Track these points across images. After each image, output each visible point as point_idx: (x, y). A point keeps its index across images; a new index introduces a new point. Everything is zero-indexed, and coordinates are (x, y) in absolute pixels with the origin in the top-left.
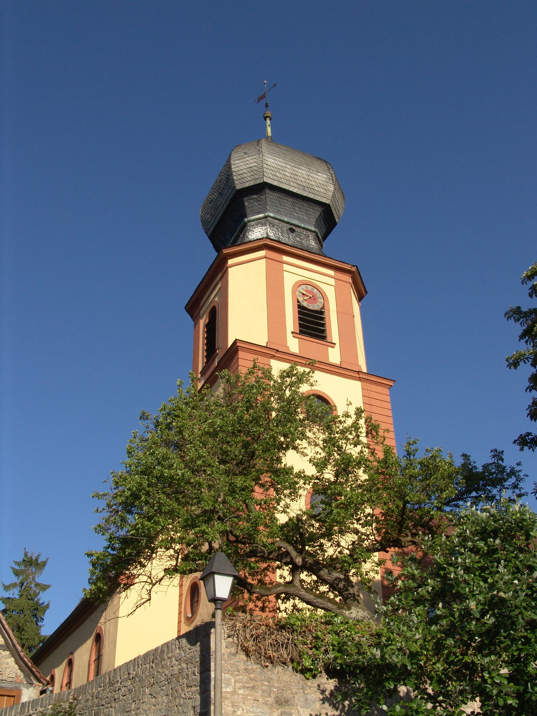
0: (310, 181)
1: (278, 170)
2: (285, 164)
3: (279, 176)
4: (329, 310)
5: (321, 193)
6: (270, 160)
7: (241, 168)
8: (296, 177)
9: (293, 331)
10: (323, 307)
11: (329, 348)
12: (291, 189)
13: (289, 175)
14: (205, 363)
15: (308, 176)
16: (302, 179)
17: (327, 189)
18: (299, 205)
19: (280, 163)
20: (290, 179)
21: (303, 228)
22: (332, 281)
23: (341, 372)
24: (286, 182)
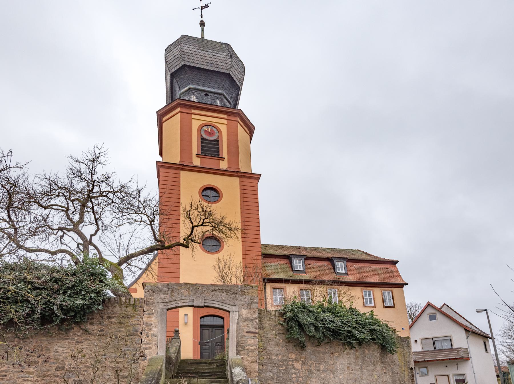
1: (192, 54)
2: (196, 50)
7: (170, 58)
8: (204, 58)
9: (197, 153)
11: (221, 161)
12: (202, 67)
14: (250, 134)
16: (209, 59)
17: (227, 63)
18: (210, 78)
20: (201, 60)
21: (215, 93)
22: (225, 122)
23: (226, 173)
24: (198, 62)
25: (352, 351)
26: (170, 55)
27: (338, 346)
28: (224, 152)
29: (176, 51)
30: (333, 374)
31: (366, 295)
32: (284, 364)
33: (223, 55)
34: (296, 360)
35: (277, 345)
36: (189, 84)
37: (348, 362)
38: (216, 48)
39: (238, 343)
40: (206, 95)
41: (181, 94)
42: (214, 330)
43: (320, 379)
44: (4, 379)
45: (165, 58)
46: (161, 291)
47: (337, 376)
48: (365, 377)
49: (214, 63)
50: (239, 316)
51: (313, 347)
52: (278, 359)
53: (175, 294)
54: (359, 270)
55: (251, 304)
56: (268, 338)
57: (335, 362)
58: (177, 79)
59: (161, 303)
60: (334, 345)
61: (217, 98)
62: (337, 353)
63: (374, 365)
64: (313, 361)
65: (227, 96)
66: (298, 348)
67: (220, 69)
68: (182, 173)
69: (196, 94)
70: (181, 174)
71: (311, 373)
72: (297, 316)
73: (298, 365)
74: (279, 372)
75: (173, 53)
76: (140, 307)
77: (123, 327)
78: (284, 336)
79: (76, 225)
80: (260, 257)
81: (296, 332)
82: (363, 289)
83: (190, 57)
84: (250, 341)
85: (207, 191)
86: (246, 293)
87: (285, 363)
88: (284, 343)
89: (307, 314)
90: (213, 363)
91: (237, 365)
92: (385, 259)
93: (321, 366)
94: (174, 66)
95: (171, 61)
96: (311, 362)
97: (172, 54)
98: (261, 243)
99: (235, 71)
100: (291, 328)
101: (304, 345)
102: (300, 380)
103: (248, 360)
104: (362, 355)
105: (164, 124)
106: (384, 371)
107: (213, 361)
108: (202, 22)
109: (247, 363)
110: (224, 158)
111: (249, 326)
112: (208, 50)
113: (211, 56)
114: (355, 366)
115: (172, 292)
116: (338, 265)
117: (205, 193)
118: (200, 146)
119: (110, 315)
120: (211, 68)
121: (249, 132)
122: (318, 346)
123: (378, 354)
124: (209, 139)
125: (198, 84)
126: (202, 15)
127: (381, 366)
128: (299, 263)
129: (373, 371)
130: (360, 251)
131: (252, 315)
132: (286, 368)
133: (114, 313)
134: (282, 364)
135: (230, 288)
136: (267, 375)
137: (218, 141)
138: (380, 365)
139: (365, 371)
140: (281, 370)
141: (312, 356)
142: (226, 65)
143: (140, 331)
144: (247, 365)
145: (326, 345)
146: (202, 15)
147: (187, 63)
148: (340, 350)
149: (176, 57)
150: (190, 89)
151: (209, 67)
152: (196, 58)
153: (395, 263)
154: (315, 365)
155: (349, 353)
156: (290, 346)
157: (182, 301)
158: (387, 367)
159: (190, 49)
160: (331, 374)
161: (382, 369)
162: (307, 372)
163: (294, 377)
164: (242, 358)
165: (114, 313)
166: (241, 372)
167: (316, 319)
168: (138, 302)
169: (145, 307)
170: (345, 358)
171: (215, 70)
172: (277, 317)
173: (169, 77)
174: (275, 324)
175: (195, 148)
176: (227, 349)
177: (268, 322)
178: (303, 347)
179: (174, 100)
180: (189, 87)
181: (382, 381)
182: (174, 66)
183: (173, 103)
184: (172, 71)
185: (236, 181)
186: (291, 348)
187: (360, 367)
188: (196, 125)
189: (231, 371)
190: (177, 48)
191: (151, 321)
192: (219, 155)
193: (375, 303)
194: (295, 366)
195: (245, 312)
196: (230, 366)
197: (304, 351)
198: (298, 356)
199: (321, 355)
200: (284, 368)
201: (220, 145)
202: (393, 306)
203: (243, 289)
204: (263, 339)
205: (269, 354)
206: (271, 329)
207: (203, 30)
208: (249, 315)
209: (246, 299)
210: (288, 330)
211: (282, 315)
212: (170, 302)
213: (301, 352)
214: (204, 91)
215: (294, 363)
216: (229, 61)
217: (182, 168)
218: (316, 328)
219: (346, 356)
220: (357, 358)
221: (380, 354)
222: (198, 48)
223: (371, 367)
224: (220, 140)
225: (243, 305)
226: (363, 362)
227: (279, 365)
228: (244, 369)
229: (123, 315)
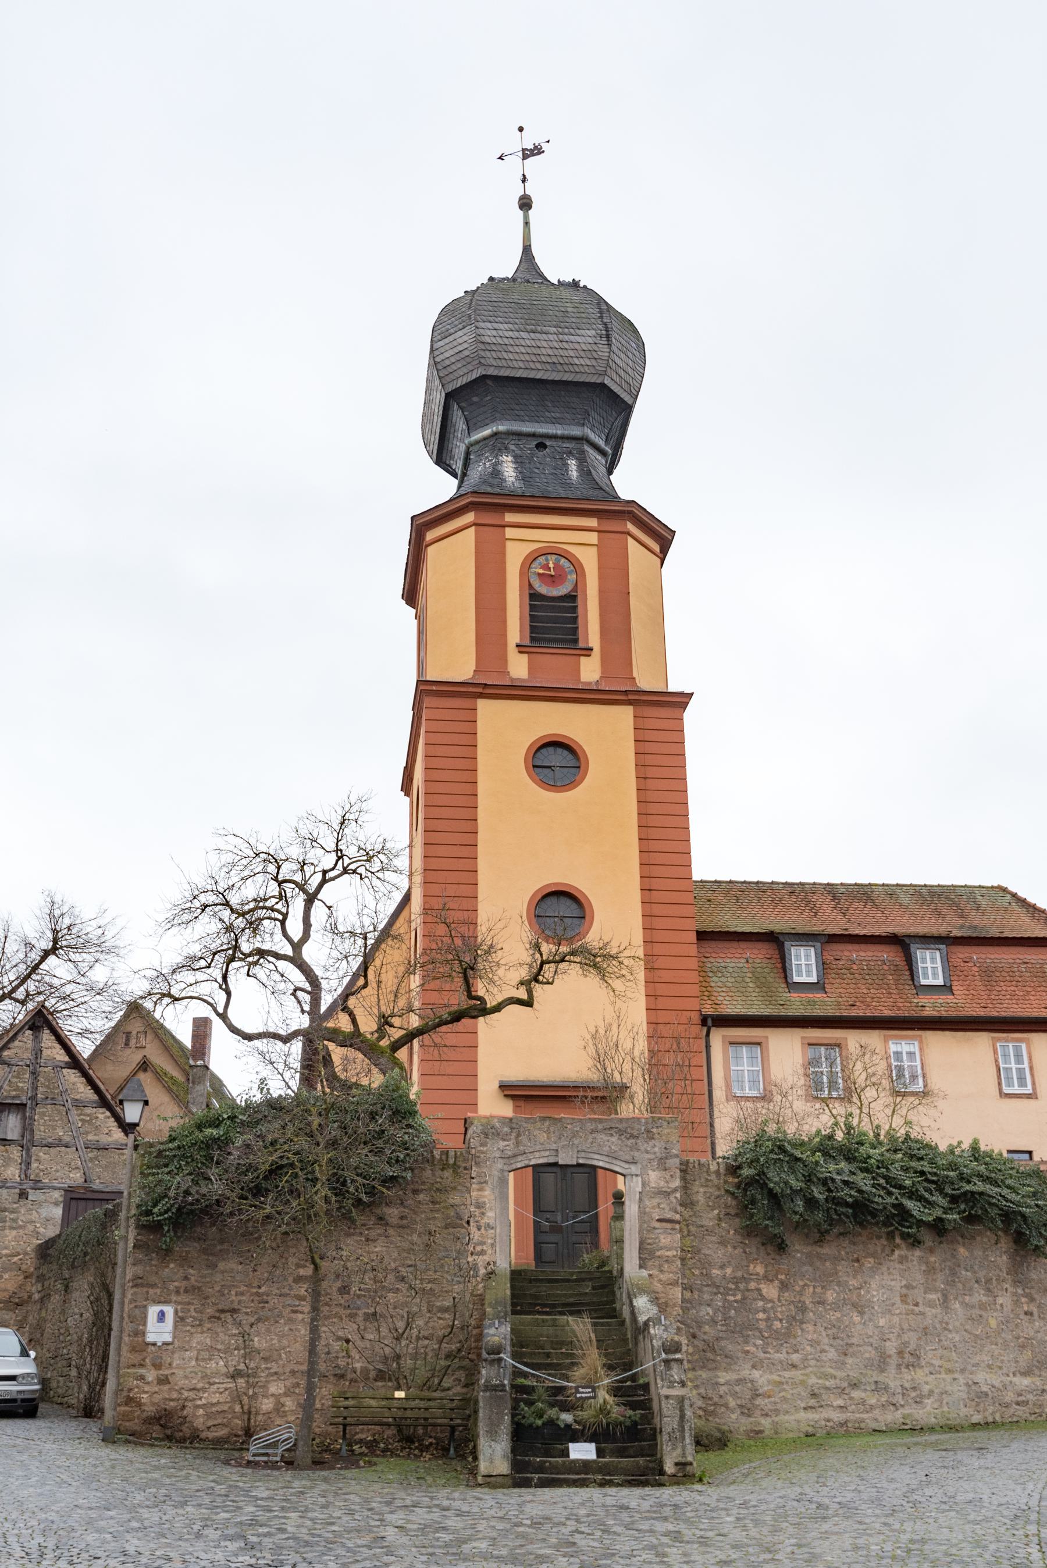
6: (489, 333)
7: (447, 355)
11: (582, 658)
12: (532, 375)
16: (550, 352)
19: (507, 334)
20: (527, 358)
21: (563, 438)
22: (593, 538)
24: (521, 364)
25: (918, 1253)
26: (447, 347)
27: (875, 1241)
28: (592, 632)
30: (861, 1313)
31: (1006, 1056)
32: (737, 1288)
33: (587, 336)
34: (767, 1278)
35: (723, 1243)
36: (494, 420)
37: (904, 1282)
38: (567, 319)
39: (641, 1243)
40: (541, 446)
41: (471, 445)
42: (569, 1175)
43: (825, 1325)
44: (263, 1307)
46: (498, 1134)
47: (870, 1320)
48: (957, 1324)
50: (644, 1184)
51: (808, 1244)
52: (724, 1277)
53: (523, 1139)
54: (988, 974)
55: (666, 1158)
56: (702, 1226)
57: (865, 1283)
58: (463, 404)
59: (500, 1160)
60: (864, 1238)
61: (570, 452)
62: (871, 1260)
63: (989, 1290)
64: (808, 1279)
66: (770, 1248)
67: (579, 376)
68: (482, 704)
69: (512, 447)
70: (479, 711)
71: (803, 1309)
72: (764, 1174)
73: (770, 1291)
74: (727, 1306)
76: (465, 1168)
77: (438, 1211)
78: (737, 1220)
79: (297, 946)
81: (761, 1215)
82: (999, 1040)
83: (499, 353)
84: (665, 1240)
86: (656, 1136)
87: (742, 1286)
88: (739, 1238)
89: (790, 1167)
90: (583, 1280)
91: (642, 1290)
93: (829, 1293)
94: (456, 374)
95: (447, 362)
96: (801, 1283)
98: (696, 877)
100: (753, 1202)
101: (783, 1241)
102: (775, 1328)
104: (948, 1263)
105: (431, 551)
106: (1026, 1308)
107: (583, 1276)
109: (658, 1287)
110: (591, 649)
111: (662, 1206)
112: (545, 329)
113: (556, 345)
114: (925, 1293)
115: (518, 1135)
116: (924, 960)
118: (528, 618)
119: (416, 1187)
120: (554, 374)
121: (656, 548)
122: (820, 1241)
123: (1004, 1258)
124: (550, 594)
125: (519, 418)
126: (524, 175)
127: (1015, 1294)
129: (982, 1306)
130: (1005, 890)
131: (667, 1182)
132: (744, 1298)
133: (423, 1183)
134: (733, 1287)
135: (624, 1125)
136: (701, 1314)
138: (1010, 1289)
139: (957, 1305)
141: (805, 1268)
142: (595, 364)
143: (466, 1218)
144: (659, 1290)
145: (841, 1238)
146: (524, 175)
147: (492, 371)
148: (879, 1252)
149: (462, 355)
150: (495, 434)
151: (549, 373)
154: (811, 1289)
155: (906, 1257)
156: (753, 1246)
157: (537, 1154)
158: (1036, 1296)
159: (500, 333)
160: (856, 1314)
161: (1017, 1303)
162: (792, 1307)
164: (650, 1275)
165: (423, 1183)
166: (649, 1305)
167: (809, 1179)
168: (461, 1159)
169: (474, 1168)
170: (894, 1272)
171: (564, 379)
172: (723, 1177)
173: (439, 397)
174: (717, 1193)
175: (515, 630)
176: (762, 1475)
177: (702, 1190)
178: (781, 1247)
181: (1018, 1338)
182: (456, 374)
184: (450, 388)
185: (625, 715)
186: (754, 1250)
187: (939, 1295)
188: (515, 555)
189: (631, 1302)
190: (465, 331)
191: (484, 1197)
192: (576, 641)
193: (1034, 1084)
194: (764, 1292)
195: (654, 1177)
196: (628, 1293)
197: (784, 1256)
198: (770, 1268)
199: (828, 1264)
200: (739, 1297)
201: (580, 610)
203: (650, 1126)
204: (692, 1229)
205: (706, 1264)
206: (709, 1206)
207: (527, 224)
208: (662, 1184)
209: (656, 1149)
210: (746, 1207)
211: (733, 1170)
212: (515, 1156)
213: (778, 1257)
214: (534, 435)
215: (762, 1286)
218: (811, 1203)
219: (897, 1266)
220: (931, 1270)
221: (1012, 1258)
222: (522, 327)
223: (979, 1296)
224: (579, 593)
225: (650, 1160)
226: (951, 1283)
227: (727, 1291)
228: (655, 1300)
229: (438, 1186)
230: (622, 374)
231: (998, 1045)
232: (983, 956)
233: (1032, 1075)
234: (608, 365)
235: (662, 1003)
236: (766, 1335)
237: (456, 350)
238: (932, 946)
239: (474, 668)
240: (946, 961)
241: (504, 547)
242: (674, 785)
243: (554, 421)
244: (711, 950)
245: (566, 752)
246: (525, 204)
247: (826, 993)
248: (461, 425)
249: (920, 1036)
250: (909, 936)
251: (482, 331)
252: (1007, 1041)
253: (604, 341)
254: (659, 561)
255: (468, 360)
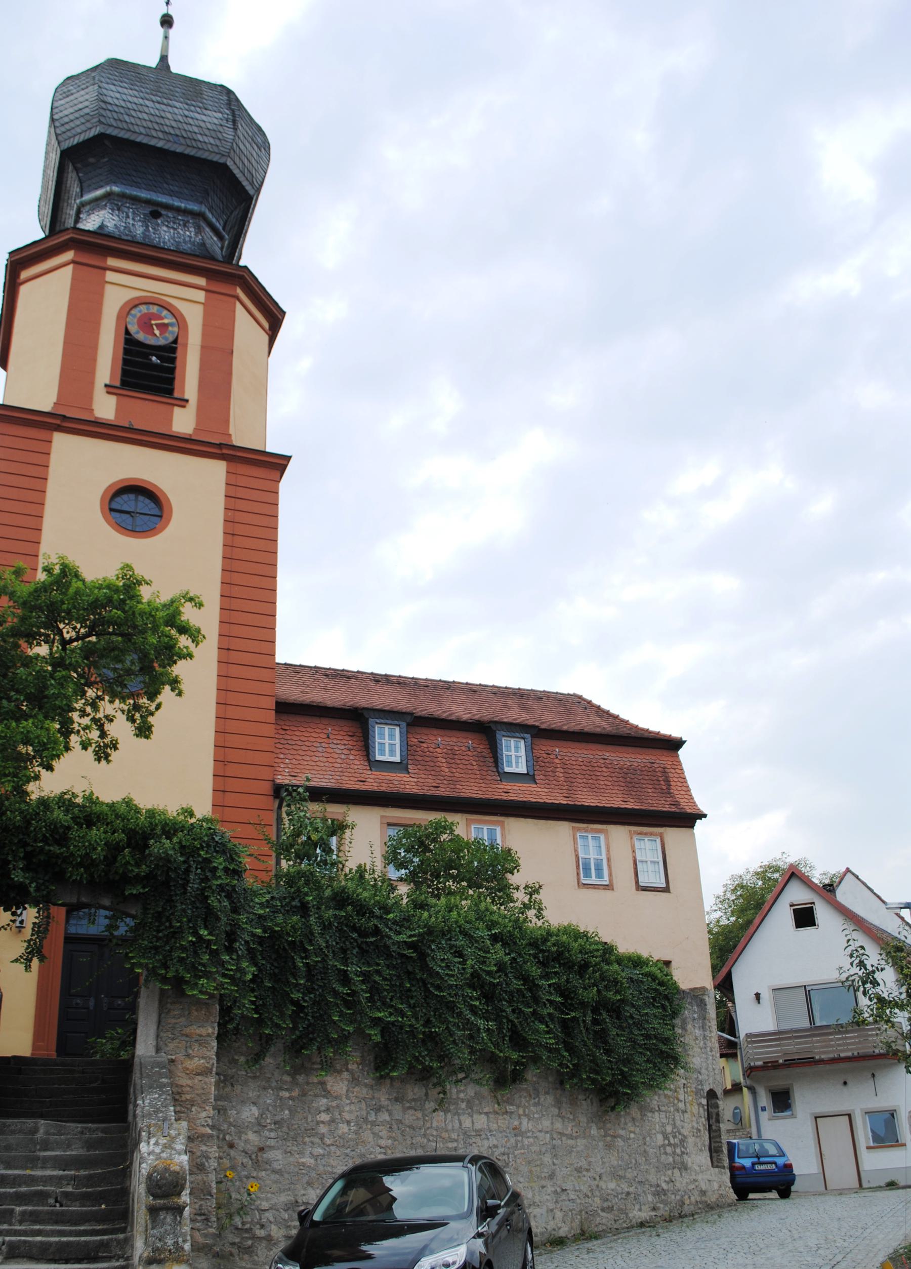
0: (189, 126)
1: (126, 110)
3: (128, 121)
4: (185, 346)
5: (209, 146)
7: (66, 112)
9: (108, 382)
10: (175, 341)
13: (147, 118)
15: (184, 118)
16: (174, 124)
17: (221, 137)
19: (130, 99)
20: (150, 125)
22: (200, 296)
26: (67, 106)
29: (86, 97)
33: (213, 118)
45: (52, 109)
49: (185, 136)
58: (79, 165)
65: (214, 220)
75: (76, 102)
80: (271, 716)
82: (579, 829)
83: (120, 115)
85: (125, 497)
92: (651, 732)
95: (66, 120)
97: (71, 104)
98: (280, 658)
99: (243, 157)
103: (188, 1069)
105: (24, 290)
108: (166, 18)
110: (187, 401)
117: (120, 503)
121: (266, 325)
125: (138, 186)
128: (392, 736)
137: (174, 350)
140: (286, 1098)
147: (109, 131)
149: (82, 113)
152: (137, 120)
153: (673, 745)
159: (124, 97)
163: (323, 1122)
171: (186, 152)
173: (55, 157)
179: (61, 231)
180: (108, 189)
183: (52, 238)
184: (66, 145)
190: (86, 90)
193: (610, 875)
202: (664, 885)
207: (166, 37)
214: (148, 202)
216: (229, 134)
217: (59, 425)
230: (246, 162)
231: (578, 835)
232: (565, 750)
233: (609, 867)
234: (232, 147)
235: (231, 770)
236: (328, 1142)
237: (76, 108)
238: (518, 735)
239: (55, 400)
240: (531, 750)
241: (103, 288)
242: (264, 582)
243: (171, 194)
244: (290, 723)
245: (147, 501)
246: (167, 22)
247: (409, 773)
248: (75, 189)
249: (503, 822)
250: (496, 722)
251: (105, 92)
252: (586, 831)
253: (230, 125)
254: (265, 338)
255: (88, 117)
